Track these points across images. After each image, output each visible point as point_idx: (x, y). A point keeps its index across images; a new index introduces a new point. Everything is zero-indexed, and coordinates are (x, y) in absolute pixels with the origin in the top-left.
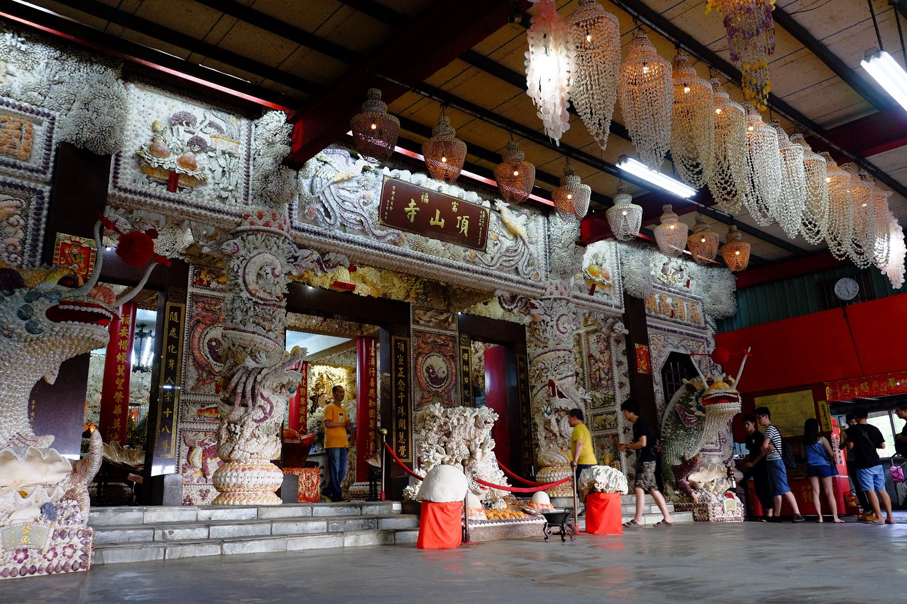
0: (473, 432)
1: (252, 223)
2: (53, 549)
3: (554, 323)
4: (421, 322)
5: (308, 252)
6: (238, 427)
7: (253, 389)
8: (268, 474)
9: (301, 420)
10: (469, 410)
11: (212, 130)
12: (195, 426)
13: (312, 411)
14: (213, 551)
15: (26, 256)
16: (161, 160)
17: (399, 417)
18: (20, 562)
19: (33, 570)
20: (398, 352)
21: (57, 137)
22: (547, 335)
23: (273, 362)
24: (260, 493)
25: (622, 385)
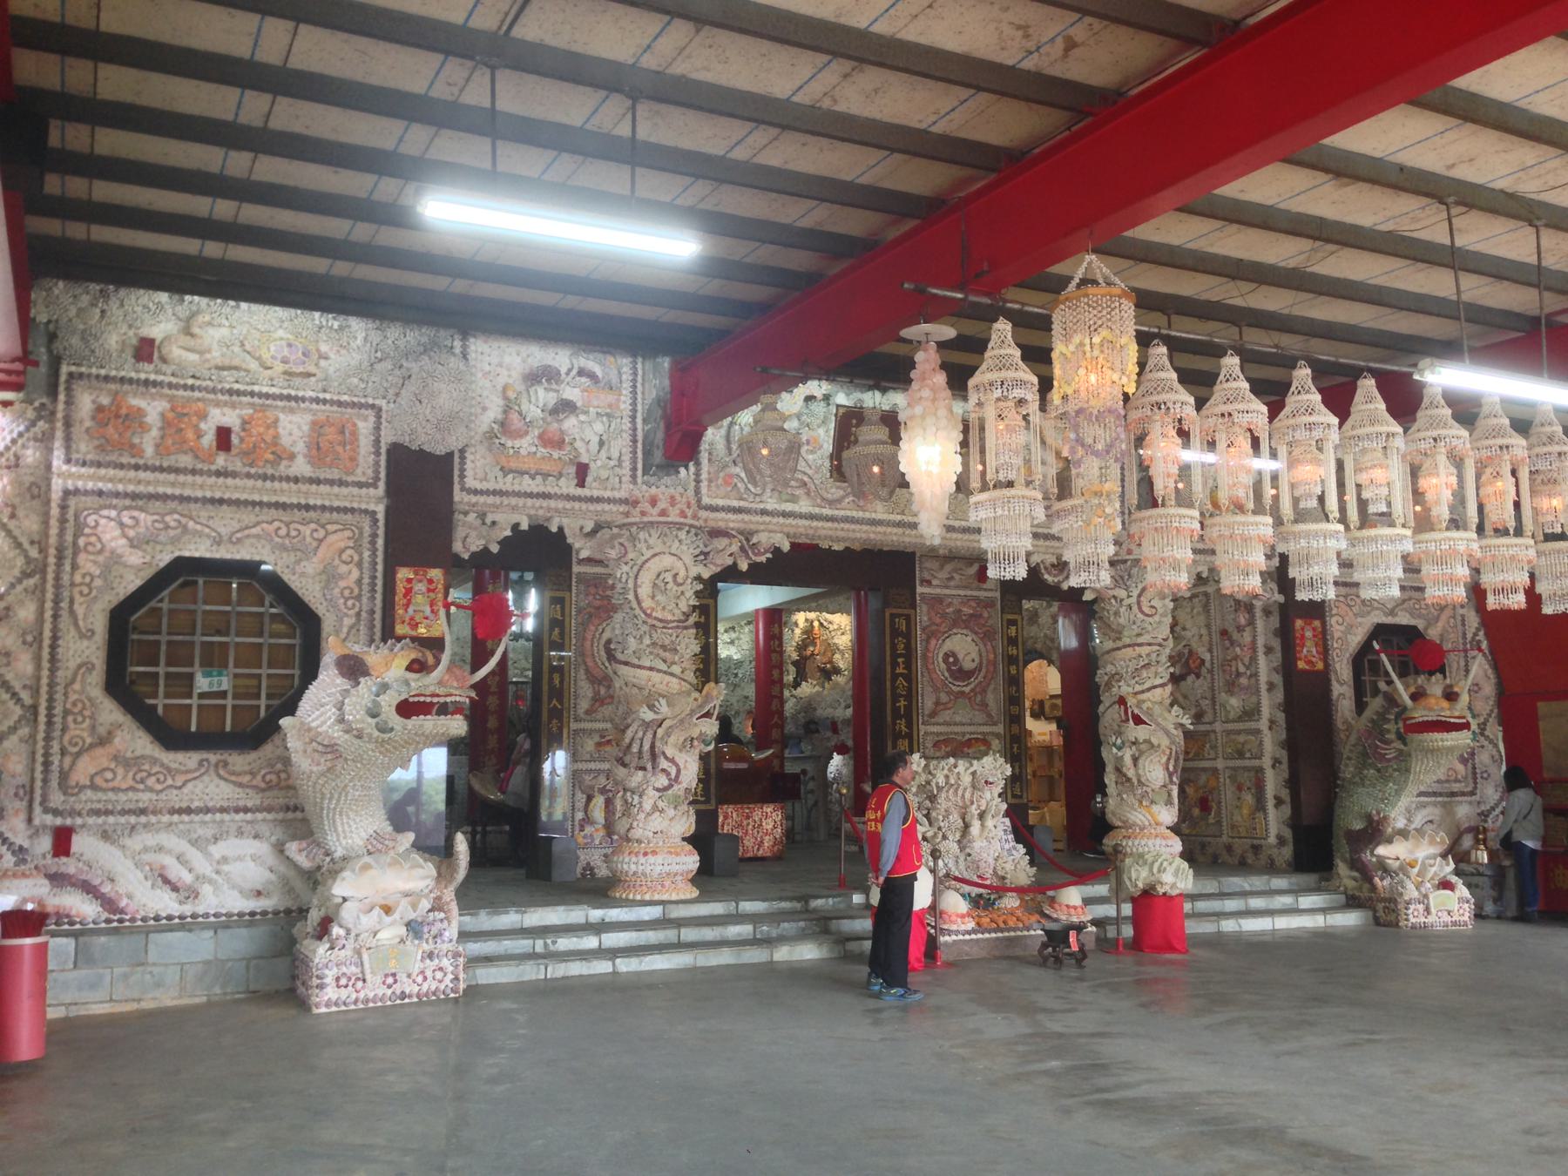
0: (968, 795)
1: (643, 513)
2: (422, 972)
3: (1133, 600)
4: (935, 582)
5: (724, 542)
6: (636, 798)
7: (653, 747)
8: (678, 859)
9: (775, 705)
10: (962, 765)
11: (583, 380)
12: (592, 766)
13: (796, 685)
14: (602, 967)
15: (365, 600)
16: (517, 443)
17: (897, 736)
18: (389, 987)
19: (403, 996)
20: (895, 633)
21: (387, 438)
22: (1122, 621)
23: (677, 710)
24: (667, 883)
25: (1271, 687)
